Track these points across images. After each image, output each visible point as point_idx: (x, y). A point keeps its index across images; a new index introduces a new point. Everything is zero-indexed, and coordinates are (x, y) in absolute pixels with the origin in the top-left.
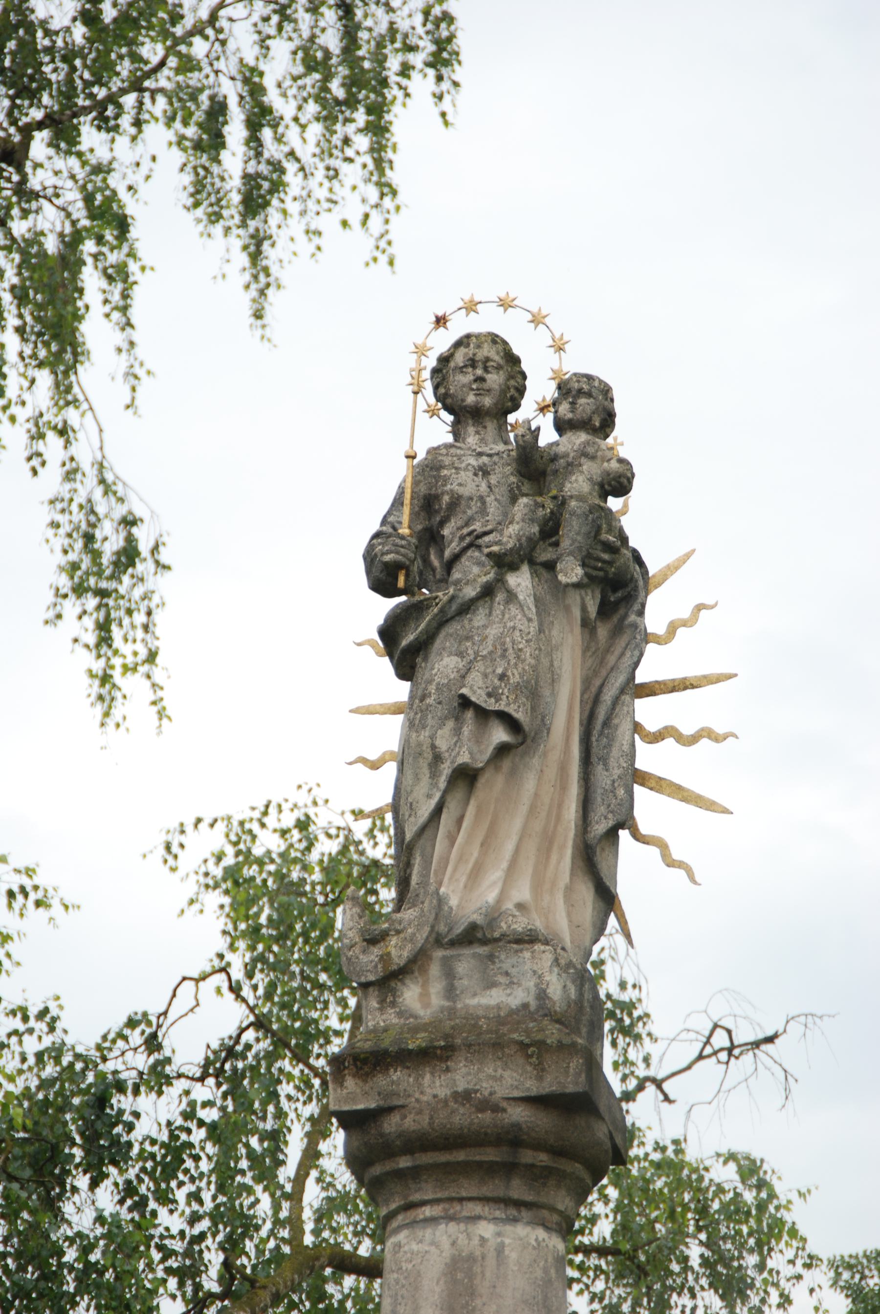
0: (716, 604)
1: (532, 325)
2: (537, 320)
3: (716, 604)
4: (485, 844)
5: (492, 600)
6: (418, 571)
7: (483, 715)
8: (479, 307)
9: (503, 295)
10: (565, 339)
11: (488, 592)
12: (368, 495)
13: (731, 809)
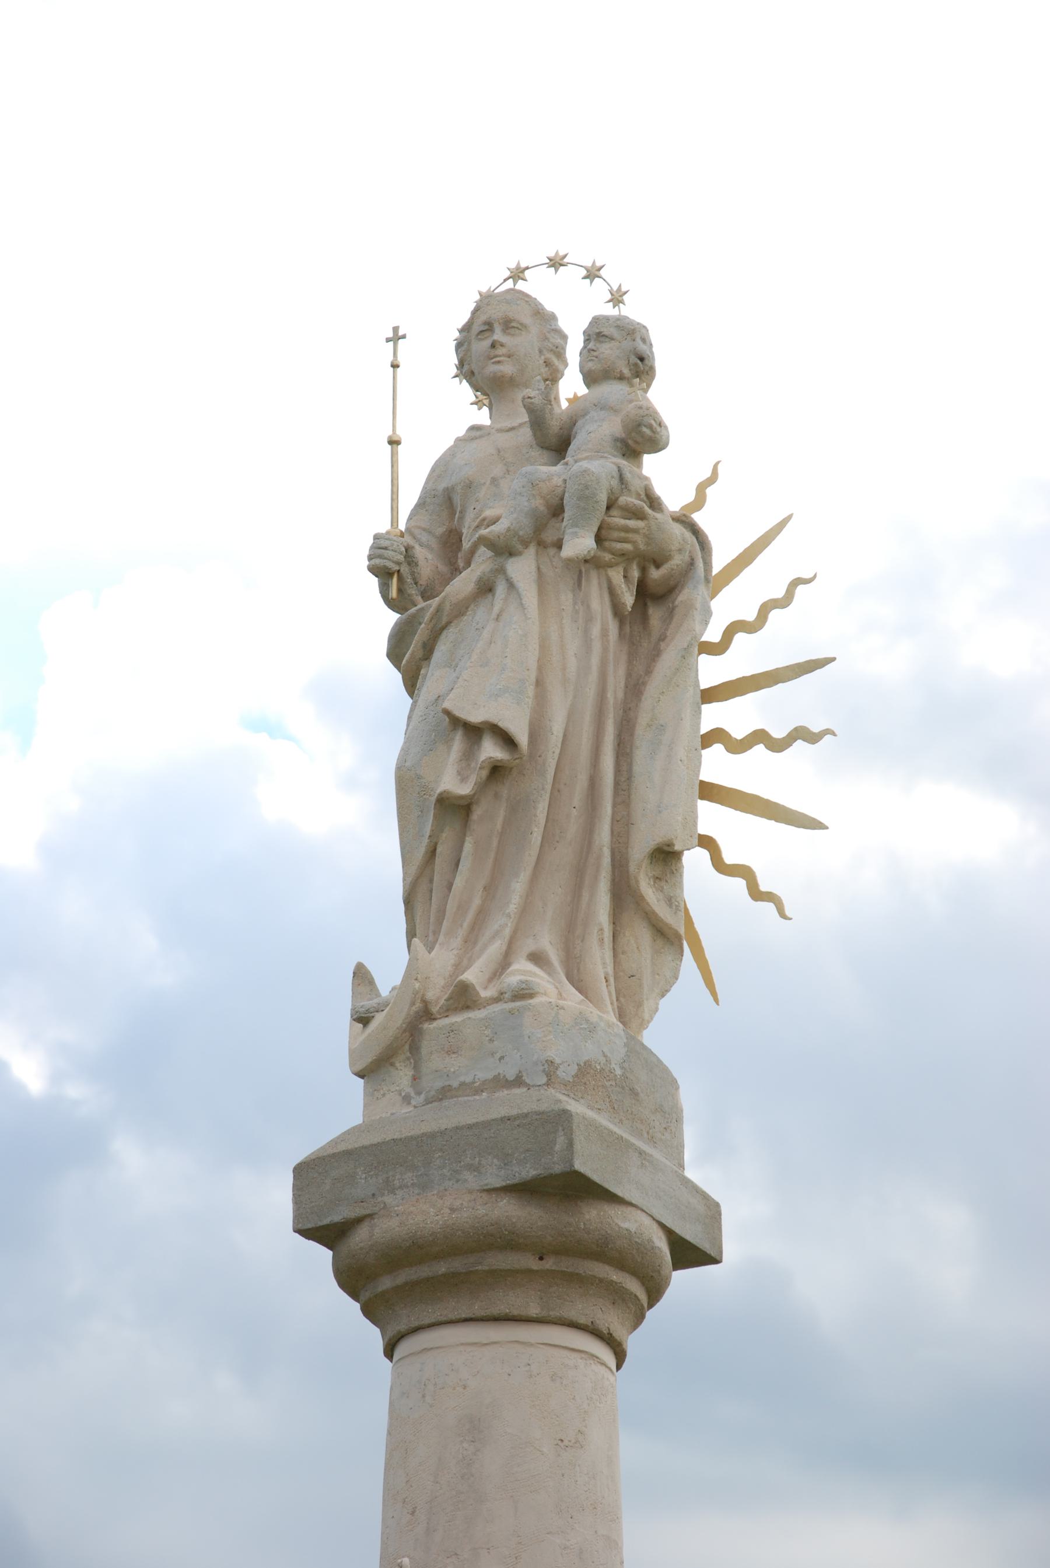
0: (815, 576)
1: (588, 281)
2: (556, 263)
3: (815, 576)
4: (490, 890)
5: (493, 595)
6: (430, 577)
7: (474, 732)
8: (527, 272)
9: (552, 254)
10: (624, 289)
11: (485, 588)
12: (375, 502)
13: (826, 824)
